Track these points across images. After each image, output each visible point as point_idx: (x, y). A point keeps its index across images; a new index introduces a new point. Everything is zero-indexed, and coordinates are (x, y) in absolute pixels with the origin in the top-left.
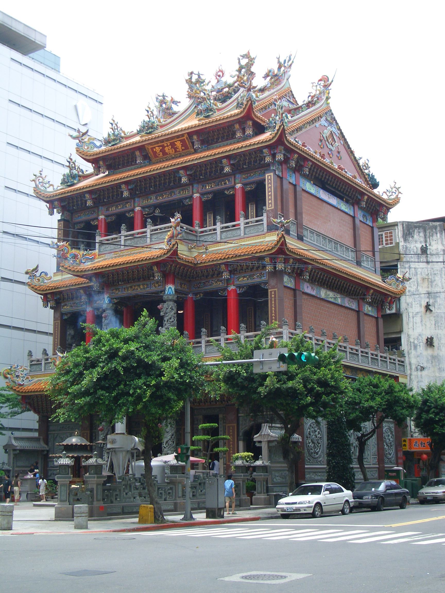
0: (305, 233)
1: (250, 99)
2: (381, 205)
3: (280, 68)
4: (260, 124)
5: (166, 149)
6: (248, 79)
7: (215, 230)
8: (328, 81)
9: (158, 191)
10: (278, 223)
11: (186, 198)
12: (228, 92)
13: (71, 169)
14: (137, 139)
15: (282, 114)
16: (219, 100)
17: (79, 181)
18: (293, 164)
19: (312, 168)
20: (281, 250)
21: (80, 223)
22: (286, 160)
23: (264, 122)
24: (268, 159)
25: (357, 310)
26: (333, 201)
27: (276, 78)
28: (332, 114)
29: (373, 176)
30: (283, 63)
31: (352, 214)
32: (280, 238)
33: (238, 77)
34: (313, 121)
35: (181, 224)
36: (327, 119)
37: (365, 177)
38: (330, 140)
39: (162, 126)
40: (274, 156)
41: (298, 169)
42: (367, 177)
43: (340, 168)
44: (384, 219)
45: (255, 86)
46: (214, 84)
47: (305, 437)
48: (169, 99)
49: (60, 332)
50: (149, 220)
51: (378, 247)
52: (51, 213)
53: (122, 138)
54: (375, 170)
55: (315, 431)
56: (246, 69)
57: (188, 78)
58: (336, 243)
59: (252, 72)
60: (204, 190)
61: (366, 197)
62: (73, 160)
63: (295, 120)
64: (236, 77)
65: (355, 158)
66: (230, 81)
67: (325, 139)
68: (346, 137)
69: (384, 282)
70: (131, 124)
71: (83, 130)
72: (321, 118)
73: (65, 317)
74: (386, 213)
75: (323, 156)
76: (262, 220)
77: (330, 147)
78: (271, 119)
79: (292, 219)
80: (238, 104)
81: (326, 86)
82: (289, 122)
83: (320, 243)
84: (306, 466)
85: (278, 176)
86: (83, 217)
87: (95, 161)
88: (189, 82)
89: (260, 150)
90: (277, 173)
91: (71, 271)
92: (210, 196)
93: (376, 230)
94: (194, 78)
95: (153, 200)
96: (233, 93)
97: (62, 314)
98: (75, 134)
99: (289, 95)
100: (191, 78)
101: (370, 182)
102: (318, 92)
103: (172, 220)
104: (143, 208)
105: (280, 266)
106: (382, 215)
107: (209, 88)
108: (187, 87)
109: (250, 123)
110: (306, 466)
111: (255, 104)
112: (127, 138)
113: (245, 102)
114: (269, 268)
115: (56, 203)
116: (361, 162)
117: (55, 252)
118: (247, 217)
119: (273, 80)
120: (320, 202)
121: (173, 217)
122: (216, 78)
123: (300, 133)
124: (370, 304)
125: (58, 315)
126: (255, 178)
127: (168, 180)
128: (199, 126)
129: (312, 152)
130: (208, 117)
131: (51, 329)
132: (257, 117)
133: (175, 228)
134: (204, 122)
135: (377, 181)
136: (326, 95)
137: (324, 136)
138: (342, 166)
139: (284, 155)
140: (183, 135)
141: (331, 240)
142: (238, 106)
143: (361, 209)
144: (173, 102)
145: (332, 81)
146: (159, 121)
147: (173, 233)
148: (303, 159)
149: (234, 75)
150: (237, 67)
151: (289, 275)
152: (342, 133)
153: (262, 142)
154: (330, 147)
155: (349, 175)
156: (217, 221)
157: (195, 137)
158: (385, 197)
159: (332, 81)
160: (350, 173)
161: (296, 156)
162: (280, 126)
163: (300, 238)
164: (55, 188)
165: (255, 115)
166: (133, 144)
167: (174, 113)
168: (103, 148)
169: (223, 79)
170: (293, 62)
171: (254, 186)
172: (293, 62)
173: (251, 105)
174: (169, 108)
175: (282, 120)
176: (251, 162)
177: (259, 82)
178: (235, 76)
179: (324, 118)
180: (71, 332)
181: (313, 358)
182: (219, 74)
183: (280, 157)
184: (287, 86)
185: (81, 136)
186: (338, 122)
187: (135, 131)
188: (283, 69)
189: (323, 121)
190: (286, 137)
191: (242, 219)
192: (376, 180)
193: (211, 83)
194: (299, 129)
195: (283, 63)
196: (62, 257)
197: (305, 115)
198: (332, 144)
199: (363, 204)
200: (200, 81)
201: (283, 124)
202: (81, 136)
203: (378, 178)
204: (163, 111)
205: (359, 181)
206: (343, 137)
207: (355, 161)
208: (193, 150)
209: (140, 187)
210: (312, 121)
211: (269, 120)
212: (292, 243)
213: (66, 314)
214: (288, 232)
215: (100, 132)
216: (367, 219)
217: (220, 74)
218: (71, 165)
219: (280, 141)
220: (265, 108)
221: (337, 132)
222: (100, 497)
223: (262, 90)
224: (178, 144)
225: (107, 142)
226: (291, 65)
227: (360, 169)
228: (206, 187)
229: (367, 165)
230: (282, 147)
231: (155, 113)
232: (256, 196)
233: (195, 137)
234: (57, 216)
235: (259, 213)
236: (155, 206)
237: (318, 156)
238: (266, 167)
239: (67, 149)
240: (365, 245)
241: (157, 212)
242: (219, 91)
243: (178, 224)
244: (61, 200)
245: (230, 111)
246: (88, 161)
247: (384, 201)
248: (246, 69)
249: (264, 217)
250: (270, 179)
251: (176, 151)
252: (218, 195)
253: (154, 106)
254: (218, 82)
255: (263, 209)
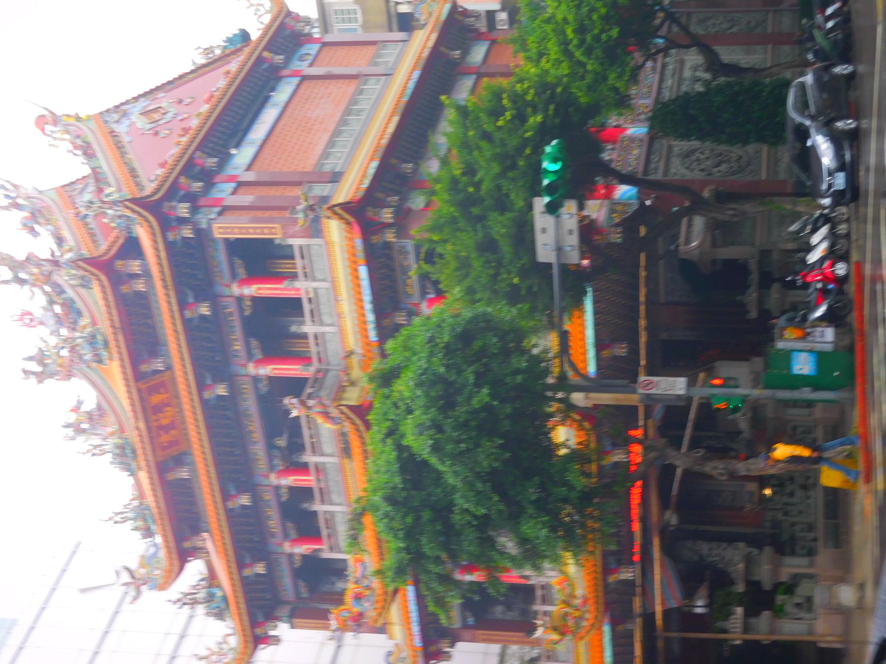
0: (327, 168)
1: (73, 262)
2: (282, 26)
3: (17, 206)
4: (122, 246)
5: (165, 422)
6: (39, 266)
7: (316, 337)
8: (43, 116)
9: (241, 441)
10: (306, 216)
11: (257, 389)
12: (63, 305)
13: (194, 603)
14: (143, 476)
15: (103, 202)
16: (75, 323)
17: (219, 586)
18: (197, 186)
19: (207, 150)
20: (358, 212)
21: (296, 587)
22: (191, 198)
23: (118, 237)
24: (187, 232)
25: (474, 77)
26: (269, 115)
27: (38, 215)
28: (108, 111)
29: (229, 40)
30: (11, 201)
31: (296, 80)
32: (336, 214)
33: (34, 285)
34: (119, 146)
35: (304, 397)
36: (117, 122)
37: (227, 55)
38: (156, 116)
39: (122, 430)
40: (182, 221)
41: (209, 178)
42: (227, 52)
43: (208, 101)
44: (308, 21)
45: (50, 253)
46: (48, 331)
47: (709, 178)
48: (72, 418)
49: (500, 631)
50: (295, 458)
51: (361, 35)
52: (276, 640)
53: (141, 504)
54: (217, 37)
55: (698, 160)
56: (22, 270)
57: (33, 379)
58: (348, 112)
59: (27, 258)
60: (243, 354)
61: (266, 54)
62: (180, 596)
63: (117, 180)
64: (35, 290)
65: (192, 72)
66: (41, 300)
67: (153, 125)
68: (153, 87)
69: (425, 25)
70: (118, 487)
71: (126, 578)
72: (113, 132)
73: (471, 621)
74: (297, 18)
75: (186, 131)
76: (301, 248)
77: (169, 116)
78: (113, 225)
79: (298, 191)
80: (82, 286)
81: (55, 120)
82: (120, 190)
83: (345, 140)
84: (764, 176)
85: (220, 214)
86: (286, 581)
87: (183, 555)
88: (40, 377)
89: (170, 246)
90: (213, 216)
91: (384, 608)
92: (254, 343)
93: (328, 38)
94: (34, 367)
95: (259, 450)
96: (64, 296)
97: (466, 627)
98: (132, 593)
99: (68, 190)
100: (34, 373)
101: (239, 46)
102: (67, 136)
103: (294, 413)
104: (272, 468)
105: (387, 215)
106: (299, 26)
107: (53, 341)
108: (49, 382)
109: (119, 263)
110: (764, 176)
111: (82, 254)
112: (141, 496)
113: (81, 273)
114: (390, 236)
115: (258, 631)
116: (202, 61)
117: (349, 636)
118: (294, 277)
119: (41, 220)
120: (273, 138)
121: (288, 412)
122: (35, 326)
123: (140, 172)
124: (466, 52)
125: (467, 634)
126: (221, 256)
127: (222, 419)
128: (121, 360)
129: (175, 151)
130: (106, 344)
131: (496, 648)
132: (109, 250)
133: (309, 408)
134: (114, 350)
135: (237, 32)
136: (72, 121)
137: (149, 126)
138: (206, 96)
139: (181, 201)
140: (139, 391)
141: (343, 122)
142: (85, 285)
143: (287, 61)
144: (76, 409)
145: (46, 109)
146: (112, 434)
147: (319, 412)
148: (189, 168)
149: (30, 294)
150: (16, 286)
151: (404, 199)
152: (146, 94)
153: (155, 241)
154: (169, 116)
155: (222, 83)
156: (299, 331)
157: (144, 368)
158: (267, 19)
159: (46, 109)
160: (218, 82)
161: (182, 180)
162: (127, 207)
163: (335, 178)
164: (230, 631)
165: (106, 253)
166: (152, 484)
167: (99, 407)
168: (159, 539)
169: (38, 313)
170: (7, 181)
171: (238, 262)
172: (7, 181)
173: (85, 260)
174: (90, 417)
175: (114, 203)
176: (191, 265)
177: (43, 246)
178: (32, 291)
179: (114, 126)
180: (499, 611)
181: (555, 150)
182: (27, 321)
183: (183, 210)
184: (55, 197)
185: (138, 582)
186: (123, 101)
187: (131, 480)
188: (20, 201)
189: (121, 129)
190: (148, 197)
191: (297, 284)
192: (235, 35)
193: (45, 337)
194: (133, 173)
195: (11, 201)
196: (358, 623)
197: (106, 163)
198: (164, 114)
199: (279, 59)
200: (40, 358)
201: (121, 202)
202: (138, 582)
203: (233, 30)
204: (93, 427)
205: (233, 66)
206: (151, 92)
207: (199, 71)
208: (168, 373)
209: (235, 472)
210: (119, 148)
211: (114, 228)
212: (345, 192)
213: (464, 619)
214: (324, 199)
215: (134, 547)
216: (307, 54)
217: (27, 318)
218: (189, 600)
219: (152, 207)
220: (92, 235)
221: (142, 104)
222: (804, 561)
223: (60, 241)
224: (156, 399)
225: (148, 533)
226: (15, 186)
227: (212, 64)
228: (236, 350)
229: (206, 49)
230: (166, 204)
231: (97, 441)
232: (261, 258)
233: (144, 368)
234: (282, 629)
235: (287, 254)
236: (271, 446)
237: (184, 139)
238: (203, 236)
239: (160, 609)
240: (356, 62)
241: (282, 442)
242: (59, 321)
243: (303, 403)
244: (254, 624)
245: (95, 299)
246: (181, 568)
247: (273, 21)
248: (22, 270)
249: (296, 242)
250: (223, 229)
251: (168, 405)
252: (251, 328)
253: (82, 443)
254: (42, 323)
255: (280, 246)
